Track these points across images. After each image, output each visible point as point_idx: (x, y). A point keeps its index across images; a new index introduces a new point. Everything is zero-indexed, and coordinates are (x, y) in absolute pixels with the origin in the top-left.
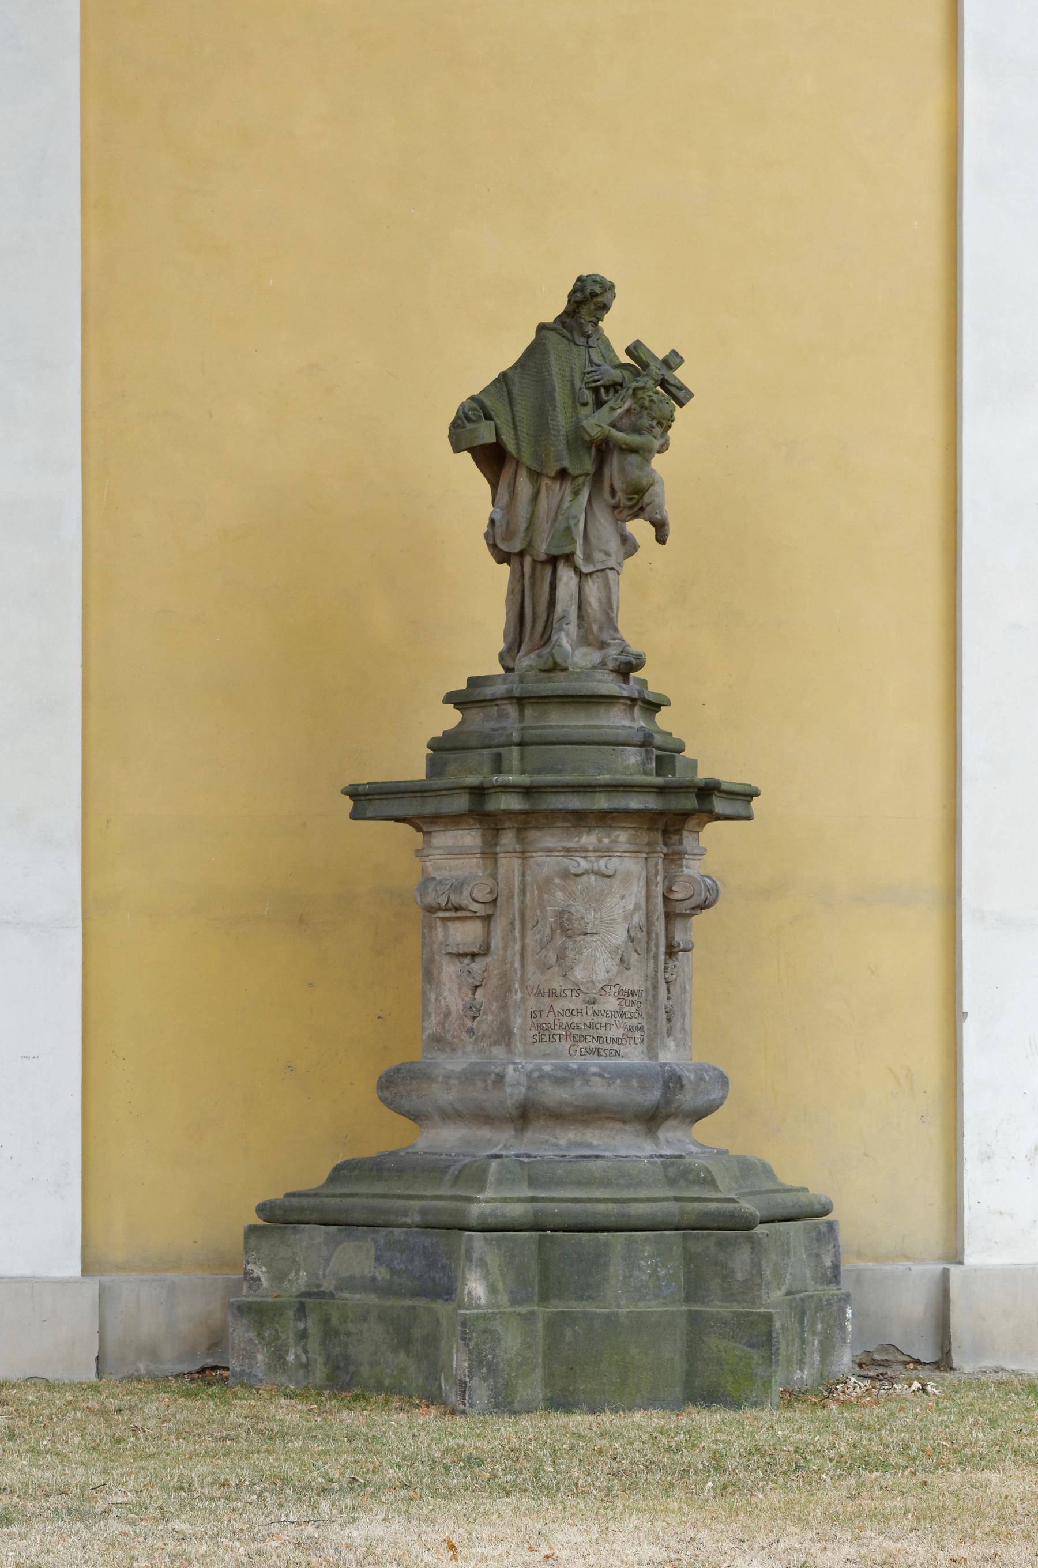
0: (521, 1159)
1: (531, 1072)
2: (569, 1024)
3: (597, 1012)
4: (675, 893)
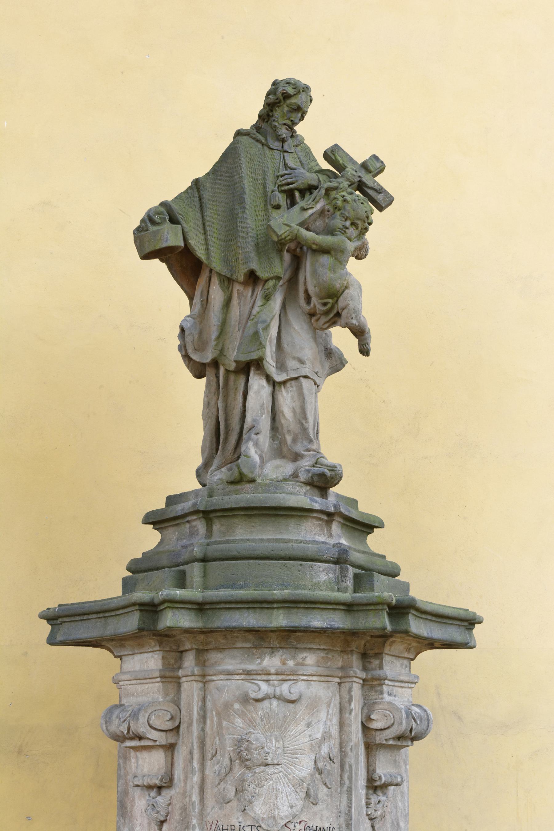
4: (374, 722)
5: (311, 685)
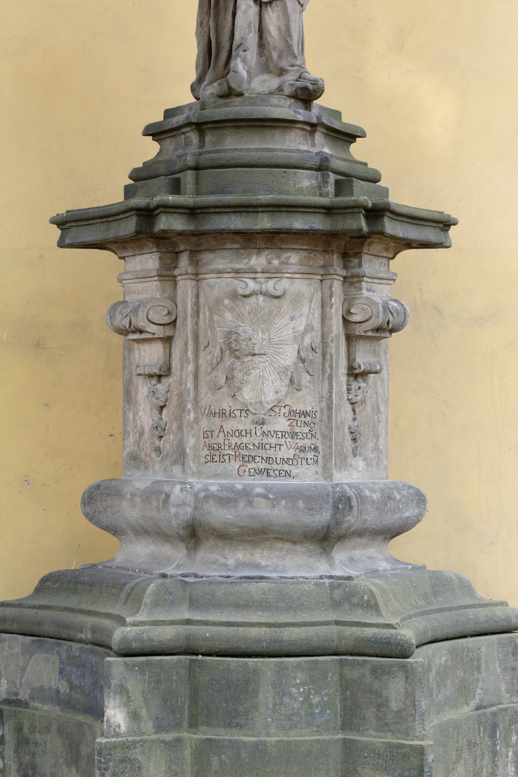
0: (186, 579)
1: (198, 492)
2: (238, 444)
3: (266, 432)
4: (354, 315)
5: (294, 282)
